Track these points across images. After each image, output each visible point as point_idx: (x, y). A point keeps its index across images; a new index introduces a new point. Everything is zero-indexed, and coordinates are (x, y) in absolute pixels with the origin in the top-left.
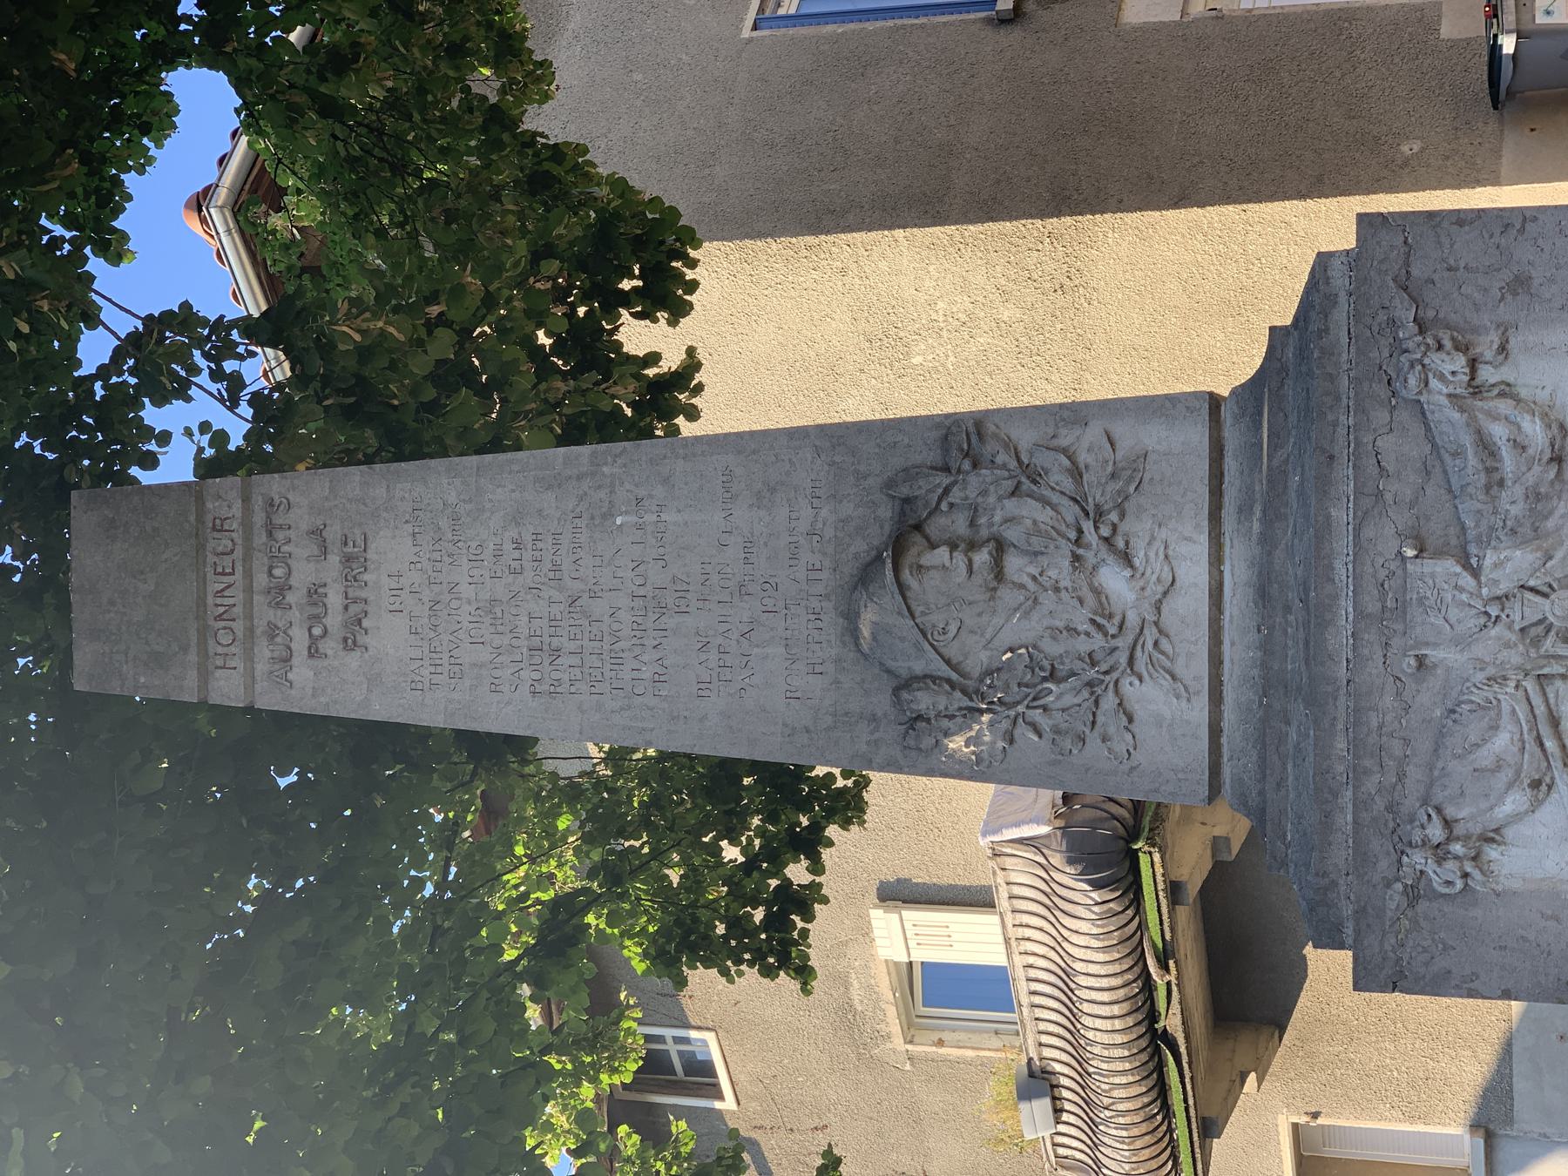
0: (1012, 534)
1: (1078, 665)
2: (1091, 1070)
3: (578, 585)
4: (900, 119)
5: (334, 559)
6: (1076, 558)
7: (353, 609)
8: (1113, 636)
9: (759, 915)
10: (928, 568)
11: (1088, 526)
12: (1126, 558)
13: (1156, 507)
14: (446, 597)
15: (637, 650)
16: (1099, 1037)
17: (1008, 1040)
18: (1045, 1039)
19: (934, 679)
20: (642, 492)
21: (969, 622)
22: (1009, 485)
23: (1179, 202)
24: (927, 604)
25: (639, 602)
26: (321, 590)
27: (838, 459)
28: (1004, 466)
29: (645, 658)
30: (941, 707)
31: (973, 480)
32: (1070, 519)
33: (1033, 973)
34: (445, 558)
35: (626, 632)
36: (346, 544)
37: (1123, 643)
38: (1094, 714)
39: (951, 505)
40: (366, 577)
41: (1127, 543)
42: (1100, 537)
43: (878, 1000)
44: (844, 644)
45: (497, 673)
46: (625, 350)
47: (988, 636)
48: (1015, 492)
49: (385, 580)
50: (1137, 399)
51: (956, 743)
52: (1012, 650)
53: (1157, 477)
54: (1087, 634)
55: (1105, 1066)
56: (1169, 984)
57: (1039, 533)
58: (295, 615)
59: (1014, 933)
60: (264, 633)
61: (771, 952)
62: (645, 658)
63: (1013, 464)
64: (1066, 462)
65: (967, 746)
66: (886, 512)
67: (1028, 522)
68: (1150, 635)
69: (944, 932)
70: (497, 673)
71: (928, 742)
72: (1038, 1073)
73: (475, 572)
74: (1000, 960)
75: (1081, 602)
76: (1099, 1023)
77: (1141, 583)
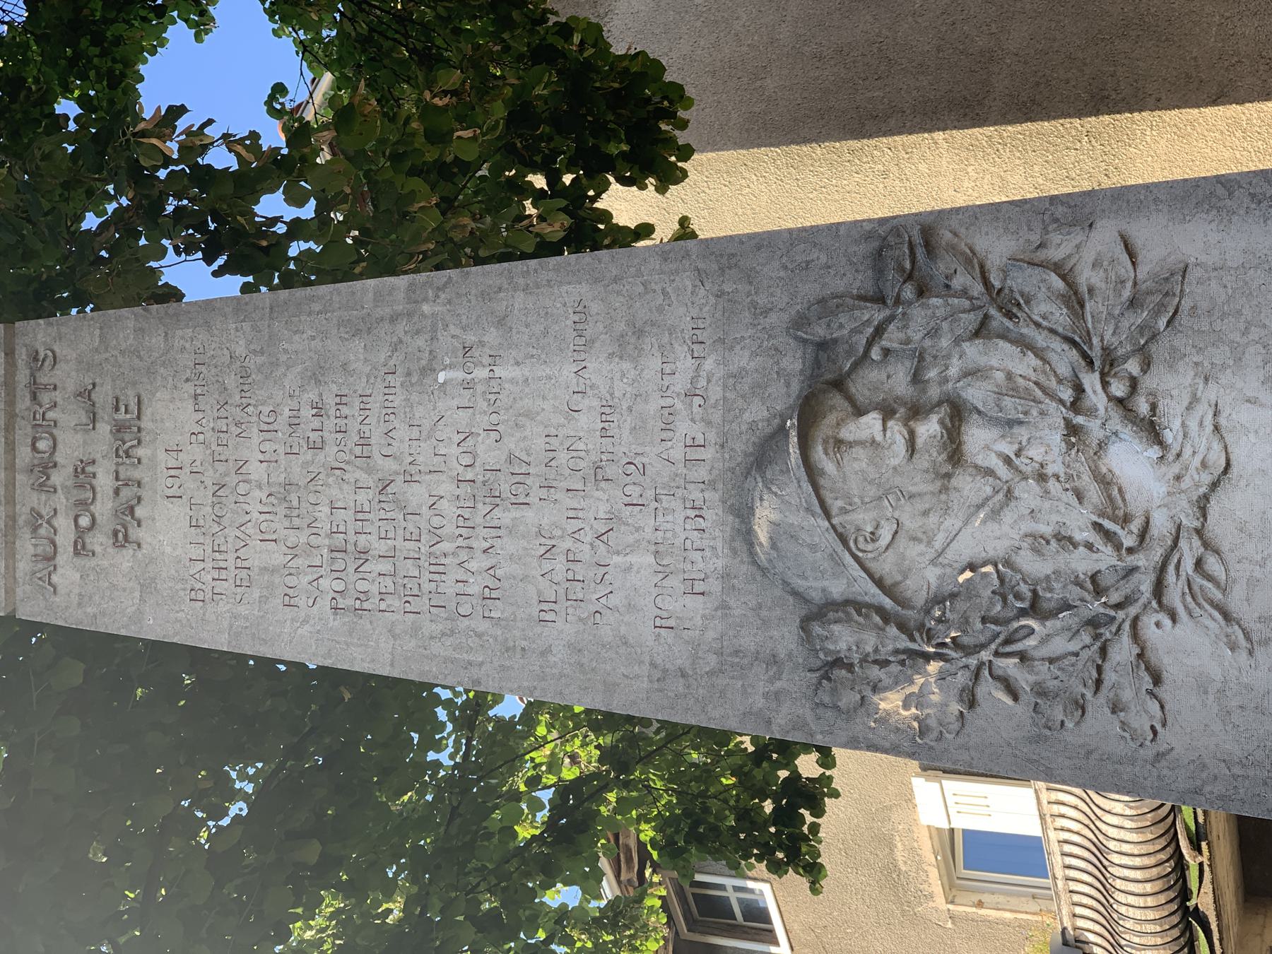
0: (975, 394)
1: (1074, 593)
2: (1123, 942)
3: (391, 465)
4: (944, 29)
5: (104, 428)
6: (1073, 430)
7: (125, 493)
8: (1130, 551)
9: (768, 807)
10: (851, 445)
11: (1091, 381)
12: (1152, 430)
13: (1200, 350)
14: (232, 479)
15: (463, 555)
16: (1131, 912)
17: (1044, 904)
18: (1079, 910)
19: (859, 606)
20: (471, 338)
21: (909, 524)
22: (970, 320)
23: (1217, 99)
24: (848, 497)
25: (466, 489)
26: (89, 469)
27: (728, 287)
28: (964, 293)
29: (473, 566)
30: (869, 649)
31: (919, 315)
32: (1064, 370)
33: (1068, 848)
34: (233, 428)
35: (450, 529)
36: (117, 409)
37: (1146, 561)
38: (1099, 669)
39: (886, 352)
40: (140, 452)
41: (1154, 407)
42: (1111, 398)
43: (920, 863)
44: (734, 552)
45: (291, 581)
46: (614, 221)
47: (938, 545)
48: (981, 331)
49: (162, 455)
50: (1170, 185)
51: (890, 702)
52: (972, 567)
53: (1204, 305)
54: (1089, 546)
55: (1136, 940)
56: (1201, 865)
57: (1014, 391)
58: (60, 500)
59: (1047, 808)
60: (27, 523)
61: (781, 847)
62: (473, 566)
63: (977, 289)
64: (1058, 284)
65: (906, 706)
66: (794, 362)
67: (1000, 376)
68: (1190, 549)
69: (983, 802)
70: (291, 581)
71: (849, 698)
72: (1072, 942)
73: (267, 446)
74: (1036, 831)
75: (1080, 496)
76: (1131, 900)
77: (1176, 469)
